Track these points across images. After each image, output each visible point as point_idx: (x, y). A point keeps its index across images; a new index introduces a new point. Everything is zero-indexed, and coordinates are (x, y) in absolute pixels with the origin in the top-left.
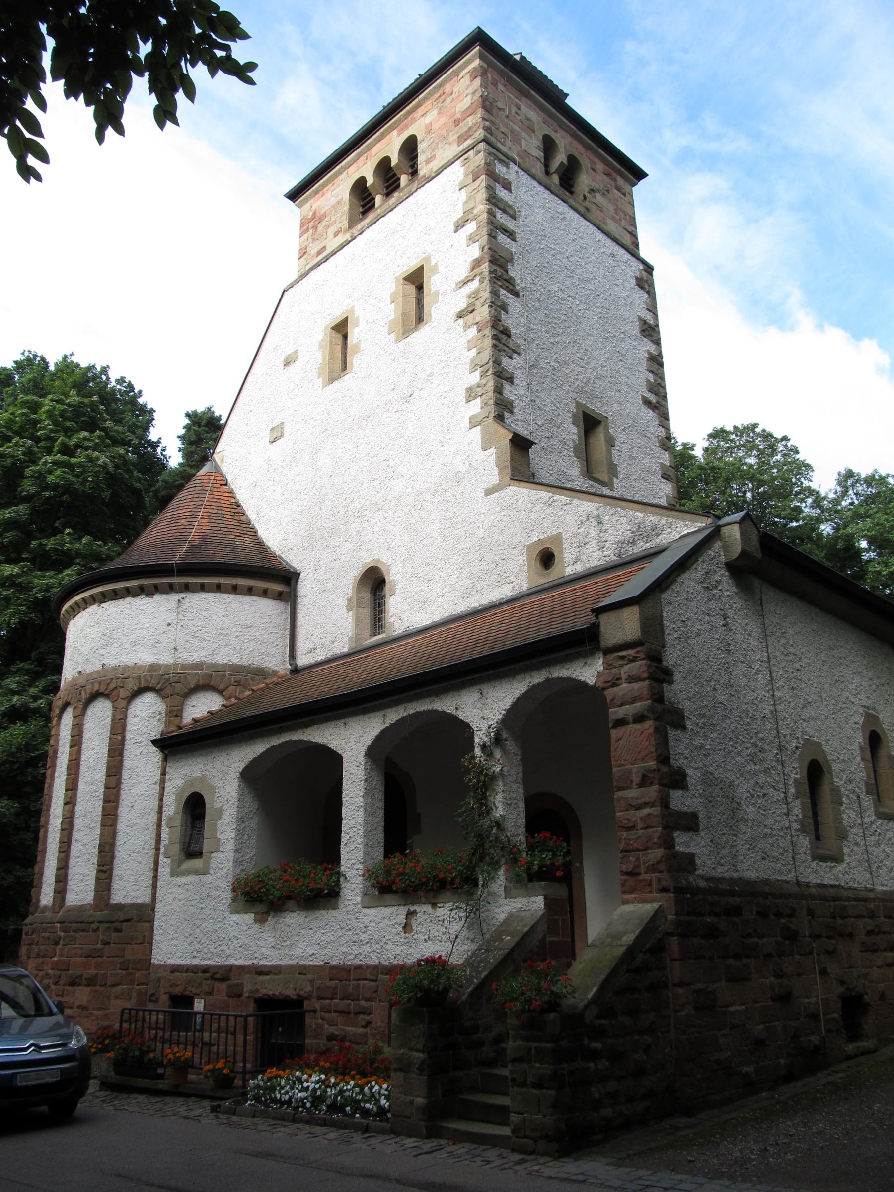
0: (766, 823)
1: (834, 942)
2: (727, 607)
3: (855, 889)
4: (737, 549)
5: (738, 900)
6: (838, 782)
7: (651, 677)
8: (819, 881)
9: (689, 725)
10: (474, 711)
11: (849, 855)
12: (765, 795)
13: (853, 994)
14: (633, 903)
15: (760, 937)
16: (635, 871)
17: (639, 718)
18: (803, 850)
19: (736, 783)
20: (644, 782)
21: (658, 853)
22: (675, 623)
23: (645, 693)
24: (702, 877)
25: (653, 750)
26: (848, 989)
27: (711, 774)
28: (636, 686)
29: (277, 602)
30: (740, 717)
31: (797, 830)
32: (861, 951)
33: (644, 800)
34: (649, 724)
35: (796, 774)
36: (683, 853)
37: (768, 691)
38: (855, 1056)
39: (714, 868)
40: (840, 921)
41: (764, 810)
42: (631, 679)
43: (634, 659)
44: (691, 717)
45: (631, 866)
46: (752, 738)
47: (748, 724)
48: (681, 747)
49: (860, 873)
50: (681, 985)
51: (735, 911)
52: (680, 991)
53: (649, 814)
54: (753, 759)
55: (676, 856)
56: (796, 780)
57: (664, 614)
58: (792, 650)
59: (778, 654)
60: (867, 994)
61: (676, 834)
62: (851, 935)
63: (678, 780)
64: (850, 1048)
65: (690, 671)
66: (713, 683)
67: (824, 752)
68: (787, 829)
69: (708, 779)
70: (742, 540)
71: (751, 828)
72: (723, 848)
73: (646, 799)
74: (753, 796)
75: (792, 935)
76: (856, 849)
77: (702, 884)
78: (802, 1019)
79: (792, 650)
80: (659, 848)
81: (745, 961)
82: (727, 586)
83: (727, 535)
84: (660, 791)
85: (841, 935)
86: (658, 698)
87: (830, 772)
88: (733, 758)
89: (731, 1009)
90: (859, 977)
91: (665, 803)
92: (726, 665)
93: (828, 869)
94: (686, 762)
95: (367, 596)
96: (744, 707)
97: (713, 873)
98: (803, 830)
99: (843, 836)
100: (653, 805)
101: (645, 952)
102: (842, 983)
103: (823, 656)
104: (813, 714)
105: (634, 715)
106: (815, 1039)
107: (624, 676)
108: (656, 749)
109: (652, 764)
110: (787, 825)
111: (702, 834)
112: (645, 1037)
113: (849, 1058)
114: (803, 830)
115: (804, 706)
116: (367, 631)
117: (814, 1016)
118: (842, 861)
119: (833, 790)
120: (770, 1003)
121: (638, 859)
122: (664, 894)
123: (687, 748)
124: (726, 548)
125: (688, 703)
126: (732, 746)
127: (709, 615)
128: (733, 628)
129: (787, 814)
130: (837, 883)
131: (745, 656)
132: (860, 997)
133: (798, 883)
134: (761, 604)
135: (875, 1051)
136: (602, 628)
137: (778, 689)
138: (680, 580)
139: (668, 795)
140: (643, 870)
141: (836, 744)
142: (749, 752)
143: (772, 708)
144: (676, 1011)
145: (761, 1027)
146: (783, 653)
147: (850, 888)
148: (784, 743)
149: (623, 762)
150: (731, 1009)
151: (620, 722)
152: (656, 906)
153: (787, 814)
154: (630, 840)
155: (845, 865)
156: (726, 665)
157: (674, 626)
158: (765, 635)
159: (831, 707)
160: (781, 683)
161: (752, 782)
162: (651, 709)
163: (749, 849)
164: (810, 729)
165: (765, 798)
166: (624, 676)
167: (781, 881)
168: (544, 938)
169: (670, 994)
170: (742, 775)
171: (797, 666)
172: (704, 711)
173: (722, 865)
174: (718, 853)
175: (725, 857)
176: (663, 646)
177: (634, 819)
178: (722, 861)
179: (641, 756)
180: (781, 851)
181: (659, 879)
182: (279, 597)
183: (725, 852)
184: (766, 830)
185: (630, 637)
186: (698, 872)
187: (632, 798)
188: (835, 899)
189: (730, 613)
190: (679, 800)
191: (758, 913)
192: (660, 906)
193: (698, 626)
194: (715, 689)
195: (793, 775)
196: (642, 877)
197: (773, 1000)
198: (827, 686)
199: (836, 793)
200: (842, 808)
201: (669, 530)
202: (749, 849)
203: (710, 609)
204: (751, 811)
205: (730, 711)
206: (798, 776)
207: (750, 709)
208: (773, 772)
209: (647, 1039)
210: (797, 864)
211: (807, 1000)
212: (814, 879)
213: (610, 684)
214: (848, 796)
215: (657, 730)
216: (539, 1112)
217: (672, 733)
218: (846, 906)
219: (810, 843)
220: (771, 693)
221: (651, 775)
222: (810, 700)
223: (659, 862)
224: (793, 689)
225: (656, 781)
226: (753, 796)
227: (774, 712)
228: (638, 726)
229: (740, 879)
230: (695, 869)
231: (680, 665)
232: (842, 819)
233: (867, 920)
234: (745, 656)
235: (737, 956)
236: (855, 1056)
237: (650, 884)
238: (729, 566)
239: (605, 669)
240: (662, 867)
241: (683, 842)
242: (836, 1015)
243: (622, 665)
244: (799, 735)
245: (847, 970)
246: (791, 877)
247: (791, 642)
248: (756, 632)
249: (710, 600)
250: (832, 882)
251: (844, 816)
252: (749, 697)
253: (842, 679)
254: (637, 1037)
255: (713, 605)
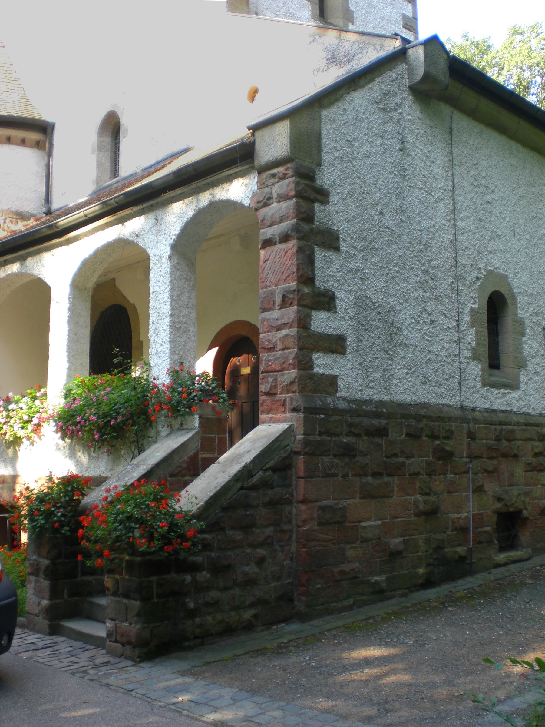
0: (431, 349)
1: (495, 462)
2: (407, 131)
3: (529, 414)
4: (420, 71)
5: (383, 421)
6: (521, 313)
7: (299, 195)
8: (487, 406)
9: (343, 247)
10: (151, 237)
11: (526, 383)
12: (432, 322)
13: (511, 510)
14: (269, 422)
15: (408, 457)
16: (272, 392)
17: (285, 238)
18: (474, 376)
19: (399, 308)
20: (285, 303)
21: (293, 374)
22: (337, 142)
23: (291, 211)
24: (344, 399)
25: (295, 270)
26: (506, 505)
27: (368, 298)
28: (284, 205)
29: (36, 150)
30: (410, 243)
31: (466, 357)
32: (526, 471)
33: (283, 321)
34: (293, 243)
35: (474, 303)
36: (322, 375)
37: (449, 221)
38: (505, 564)
39: (361, 390)
40: (505, 443)
41: (430, 337)
42: (282, 198)
43: (284, 177)
44: (348, 239)
45: (269, 387)
46: (423, 265)
47: (421, 251)
48: (329, 269)
49: (537, 400)
50: (303, 502)
51: (382, 432)
52: (303, 507)
53: (287, 335)
54: (422, 285)
55: (313, 377)
56: (472, 310)
57: (324, 132)
58: (483, 182)
59: (466, 184)
60: (526, 509)
61: (315, 356)
62: (516, 456)
63: (326, 301)
64: (502, 557)
65: (351, 193)
66: (379, 207)
67: (509, 284)
68: (455, 356)
69: (362, 303)
70: (425, 61)
71: (412, 353)
72: (375, 371)
73: (285, 320)
74: (418, 323)
75: (445, 456)
76: (535, 378)
77: (342, 405)
78: (449, 533)
79: (483, 182)
80: (294, 369)
81: (386, 479)
82: (410, 111)
83: (412, 58)
84: (298, 312)
85: (505, 456)
86: (305, 217)
87: (515, 304)
88: (397, 283)
89: (364, 524)
90: (519, 494)
91: (303, 323)
92: (399, 190)
93: (500, 396)
94: (336, 284)
95: (108, 140)
96: (417, 234)
97: (359, 395)
98: (475, 357)
99: (522, 364)
100: (291, 327)
101: (266, 470)
102: (499, 500)
103: (521, 192)
104: (501, 247)
105: (280, 234)
106: (461, 550)
107: (275, 195)
108: (298, 269)
109: (293, 284)
110: (457, 352)
111: (350, 357)
112: (258, 550)
113: (498, 566)
114: (475, 357)
115: (492, 238)
116: (108, 174)
117: (464, 530)
118: (518, 388)
119: (516, 321)
120: (413, 518)
121: (276, 379)
122: (295, 414)
123: (338, 271)
124: (411, 71)
125: (344, 225)
126: (397, 272)
127: (382, 137)
128: (413, 154)
129: (458, 342)
130: (509, 409)
131: (425, 183)
132: (520, 512)
133: (462, 407)
134: (451, 133)
135: (527, 559)
136: (257, 146)
137: (462, 219)
138: (349, 97)
139: (309, 316)
140: (279, 390)
141: (526, 278)
142: (418, 279)
143: (452, 237)
144: (298, 526)
145: (399, 540)
146: (472, 184)
147: (523, 413)
148: (462, 273)
149: (268, 283)
150: (364, 524)
151: (268, 243)
152: (286, 425)
153: (458, 342)
154: (269, 361)
155: (520, 392)
156: (399, 190)
157: (336, 145)
158: (451, 163)
159: (524, 242)
160: (466, 214)
161: (419, 309)
162: (296, 228)
163: (407, 373)
164: (497, 263)
165: (434, 325)
166: (275, 195)
167: (443, 405)
168: (196, 455)
169: (294, 510)
170: (406, 301)
171: (489, 198)
172: (365, 234)
173: (371, 388)
174: (367, 376)
175: (376, 380)
176: (319, 165)
177: (274, 340)
178: (372, 384)
179: (284, 277)
180: (446, 376)
181: (292, 399)
182: (38, 145)
183: (377, 375)
184: (430, 356)
185: (280, 153)
186: (338, 394)
187: (274, 319)
188: (501, 423)
189: (410, 138)
190: (321, 322)
191: (408, 435)
192: (290, 427)
193: (367, 147)
194: (381, 213)
195: (469, 305)
196: (278, 397)
197: (416, 515)
198: (521, 221)
199: (520, 324)
200: (524, 339)
201: (360, 55)
202: (407, 373)
203: (386, 132)
204: (414, 337)
205: (399, 236)
206: (476, 306)
207: (425, 237)
208: (446, 300)
209: (261, 552)
210: (464, 389)
211: (456, 516)
212: (481, 404)
213: (261, 204)
214: (532, 328)
215: (300, 250)
216: (127, 620)
217: (320, 254)
218: (514, 430)
219: (482, 370)
220: (453, 222)
221: (291, 296)
222: (500, 233)
223: (292, 383)
224: (480, 220)
225: (295, 302)
226: (418, 323)
227: (454, 242)
228: (283, 246)
229: (392, 402)
230: (337, 391)
231: (339, 185)
232: (523, 349)
233: (537, 443)
234: (425, 183)
235: (375, 475)
236: (505, 564)
237: (284, 405)
238: (414, 90)
239: (259, 188)
240: (295, 387)
241: (323, 364)
242: (489, 529)
243: (273, 184)
244: (482, 266)
245: (507, 488)
246: (454, 401)
247: (484, 174)
248: (441, 158)
249: (385, 123)
250: (503, 408)
251: (526, 346)
252: (426, 223)
253: (540, 216)
254: (248, 551)
255: (389, 128)
